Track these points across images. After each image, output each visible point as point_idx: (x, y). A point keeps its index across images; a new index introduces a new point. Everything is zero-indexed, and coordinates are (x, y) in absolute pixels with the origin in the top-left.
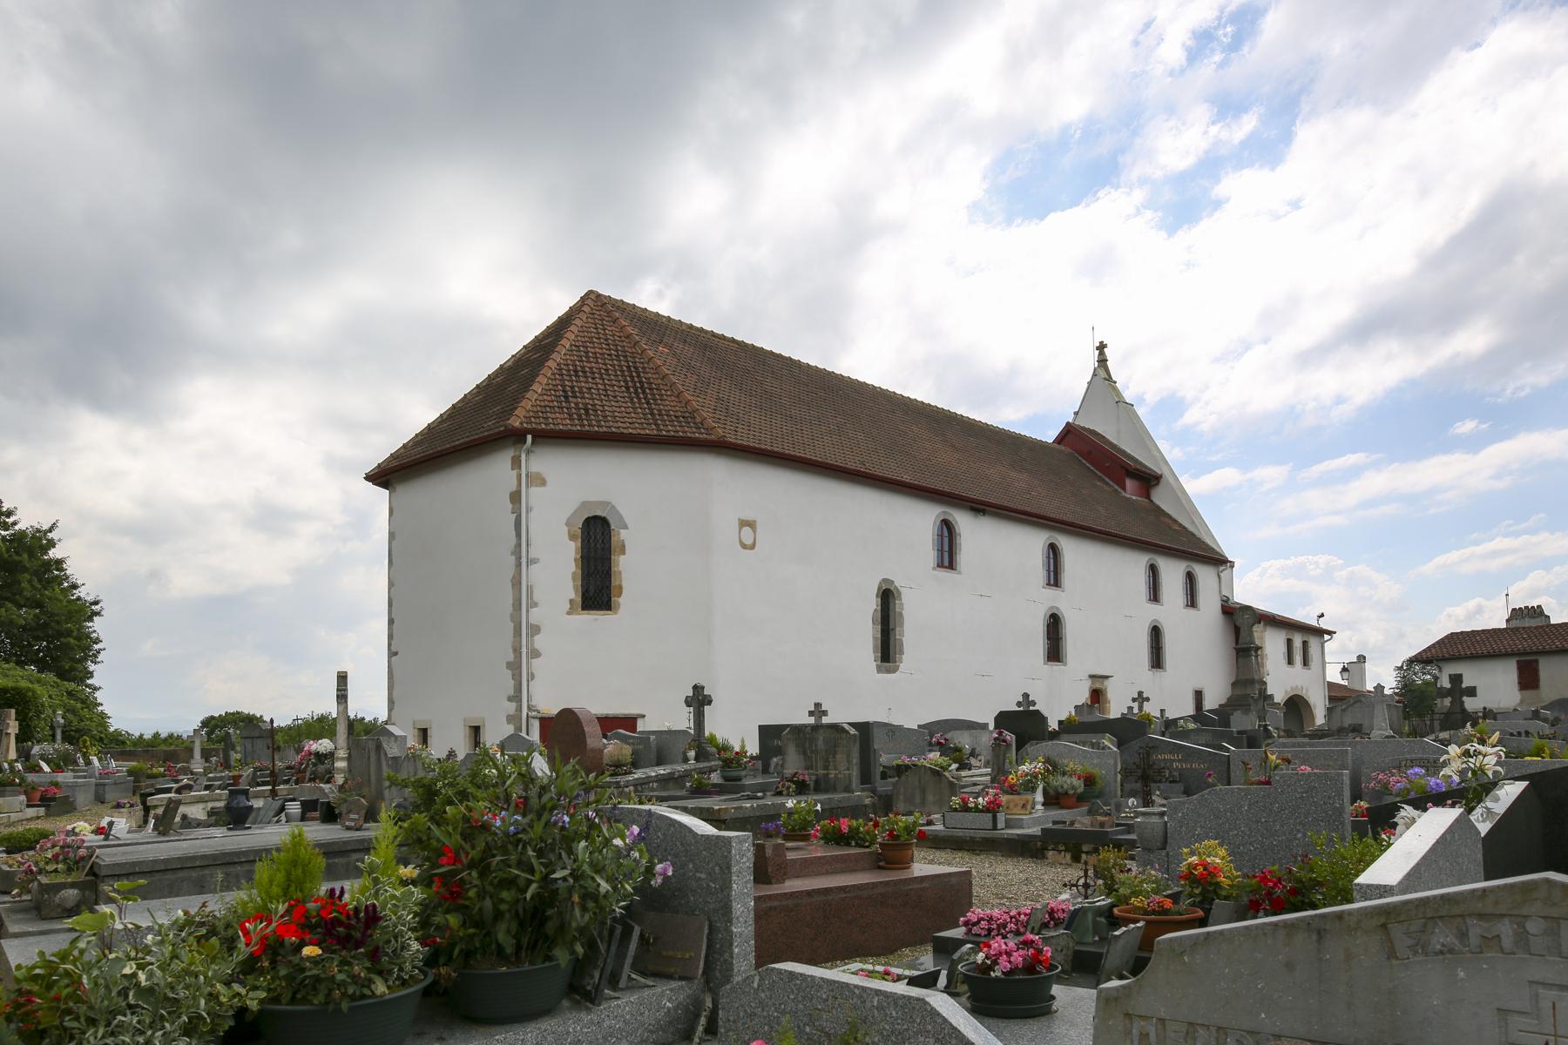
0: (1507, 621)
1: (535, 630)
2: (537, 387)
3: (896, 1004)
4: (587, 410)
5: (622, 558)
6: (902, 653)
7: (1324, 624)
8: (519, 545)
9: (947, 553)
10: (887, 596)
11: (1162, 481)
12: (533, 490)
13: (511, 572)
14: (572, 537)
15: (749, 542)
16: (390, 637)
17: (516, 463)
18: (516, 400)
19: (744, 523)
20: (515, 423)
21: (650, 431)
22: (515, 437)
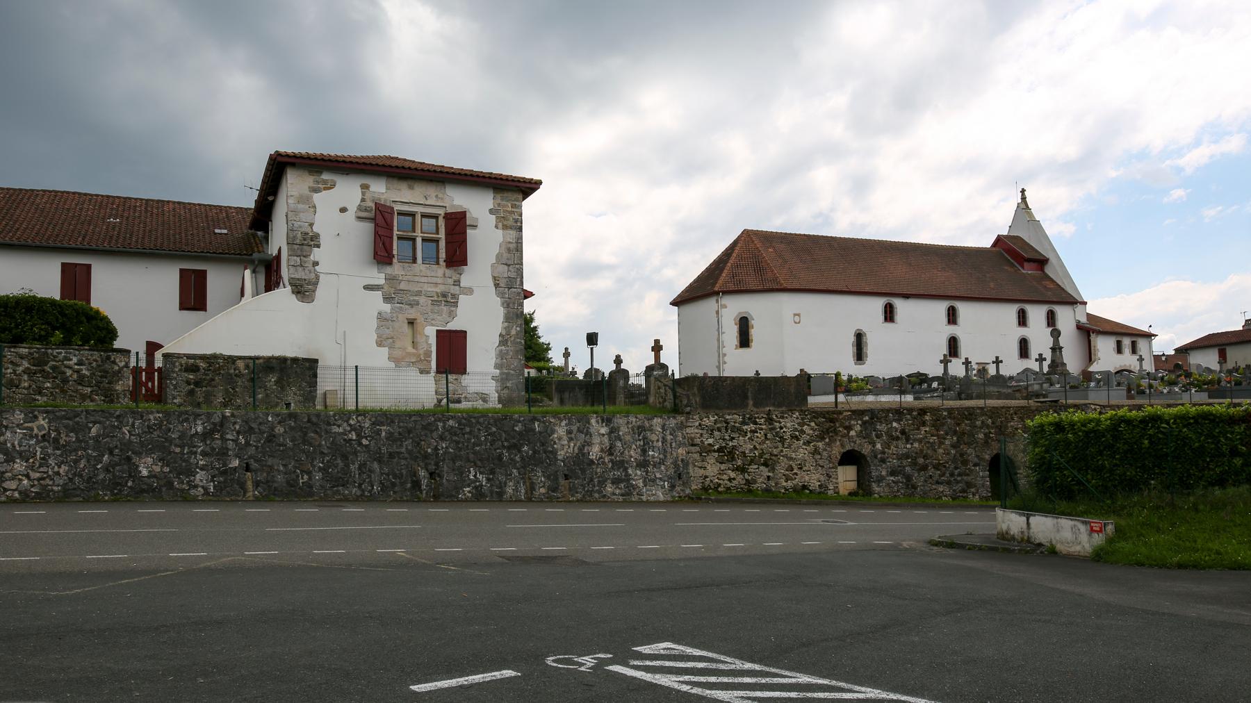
0: (1243, 326)
1: (725, 355)
2: (724, 275)
3: (184, 208)
4: (740, 281)
5: (752, 330)
6: (867, 357)
7: (1153, 331)
8: (719, 328)
9: (889, 314)
10: (859, 337)
11: (1050, 261)
12: (723, 310)
13: (716, 336)
14: (736, 324)
15: (798, 321)
16: (679, 358)
17: (717, 301)
18: (717, 279)
19: (795, 315)
20: (716, 289)
21: (760, 287)
22: (717, 293)
